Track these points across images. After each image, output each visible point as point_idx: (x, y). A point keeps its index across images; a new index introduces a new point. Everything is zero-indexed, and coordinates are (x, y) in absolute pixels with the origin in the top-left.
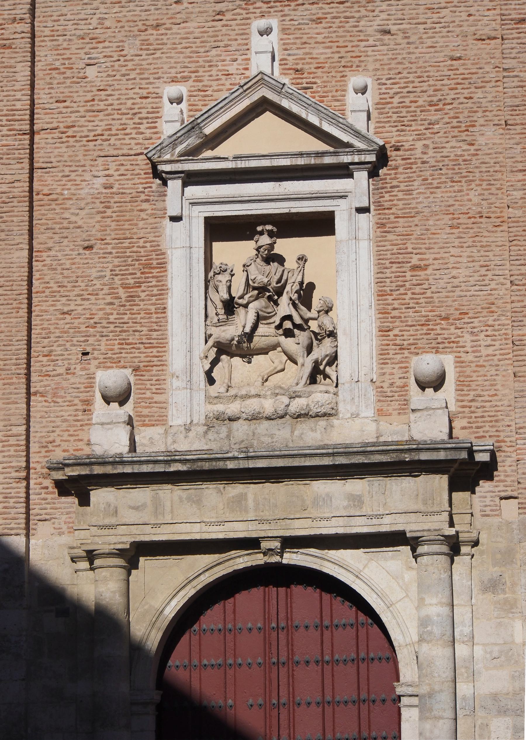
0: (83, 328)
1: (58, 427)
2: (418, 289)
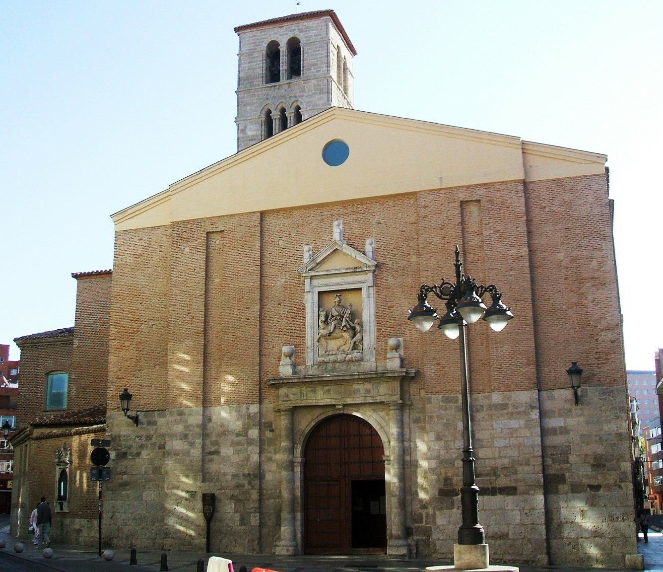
0: (278, 332)
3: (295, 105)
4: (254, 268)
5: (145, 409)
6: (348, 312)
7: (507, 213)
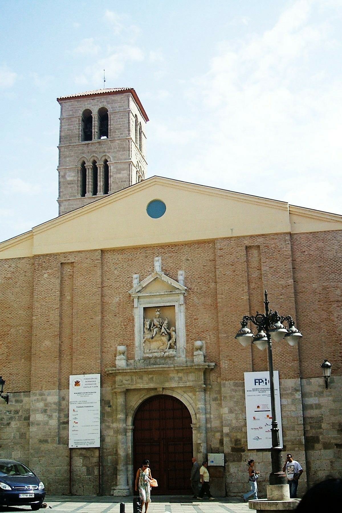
2: (196, 325)
3: (103, 159)
4: (96, 290)
5: (13, 391)
6: (166, 322)
7: (278, 255)
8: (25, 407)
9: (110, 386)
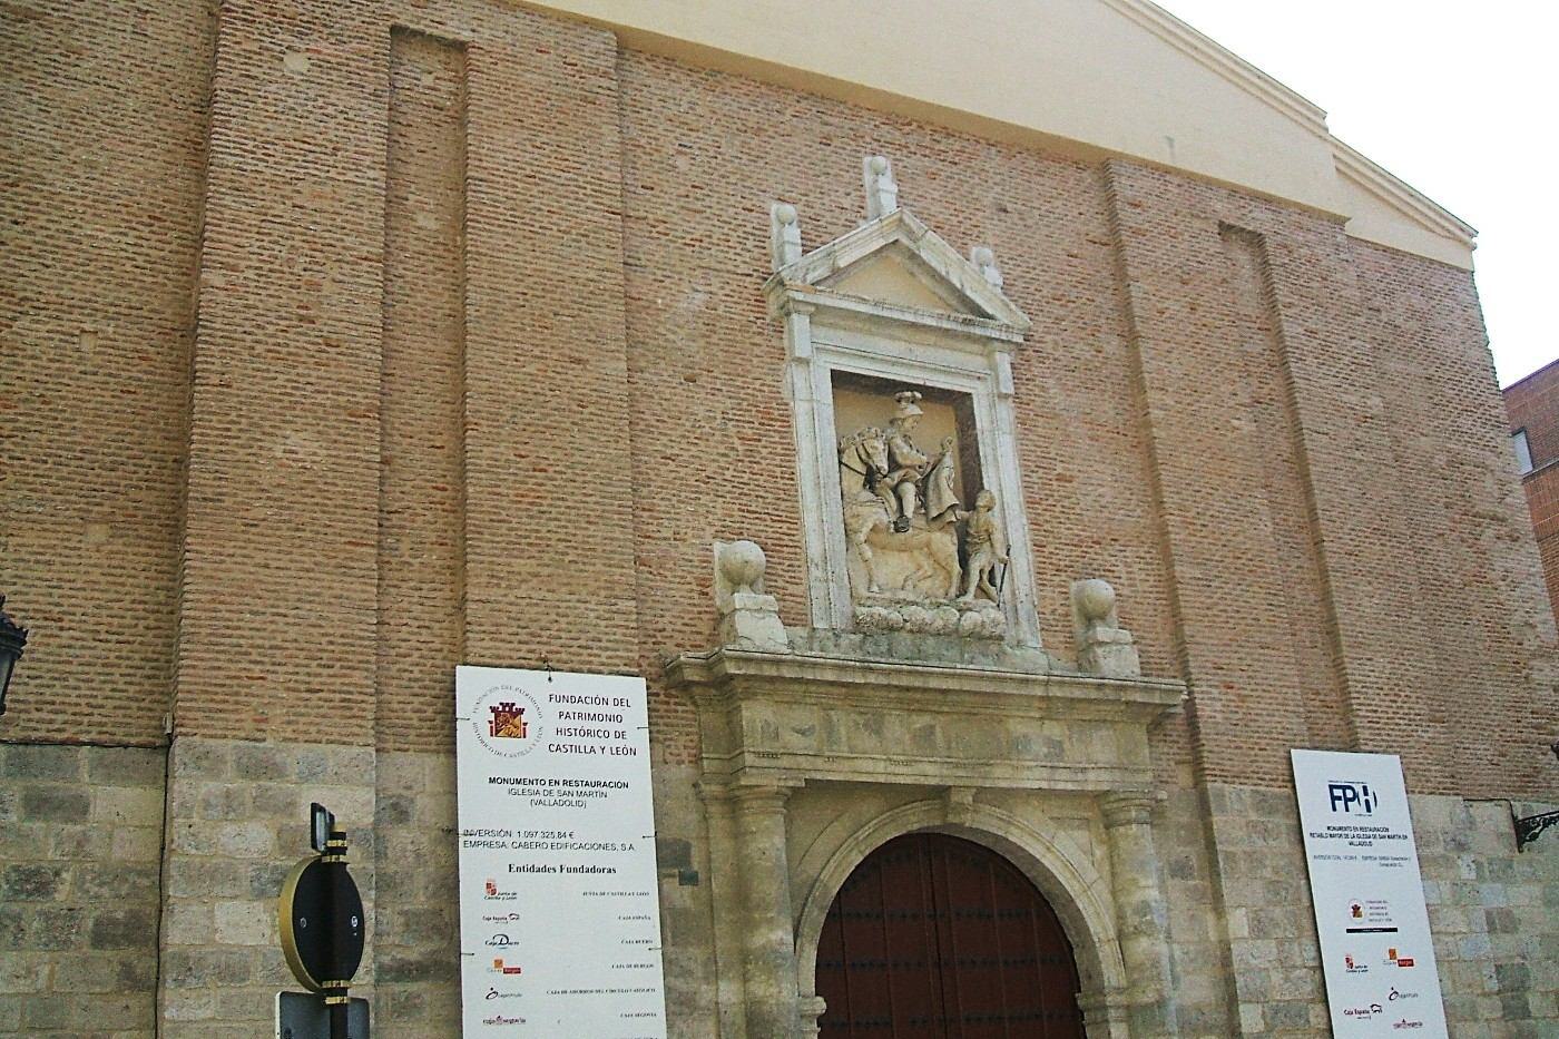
1: (669, 610)
8: (99, 853)
9: (685, 756)
